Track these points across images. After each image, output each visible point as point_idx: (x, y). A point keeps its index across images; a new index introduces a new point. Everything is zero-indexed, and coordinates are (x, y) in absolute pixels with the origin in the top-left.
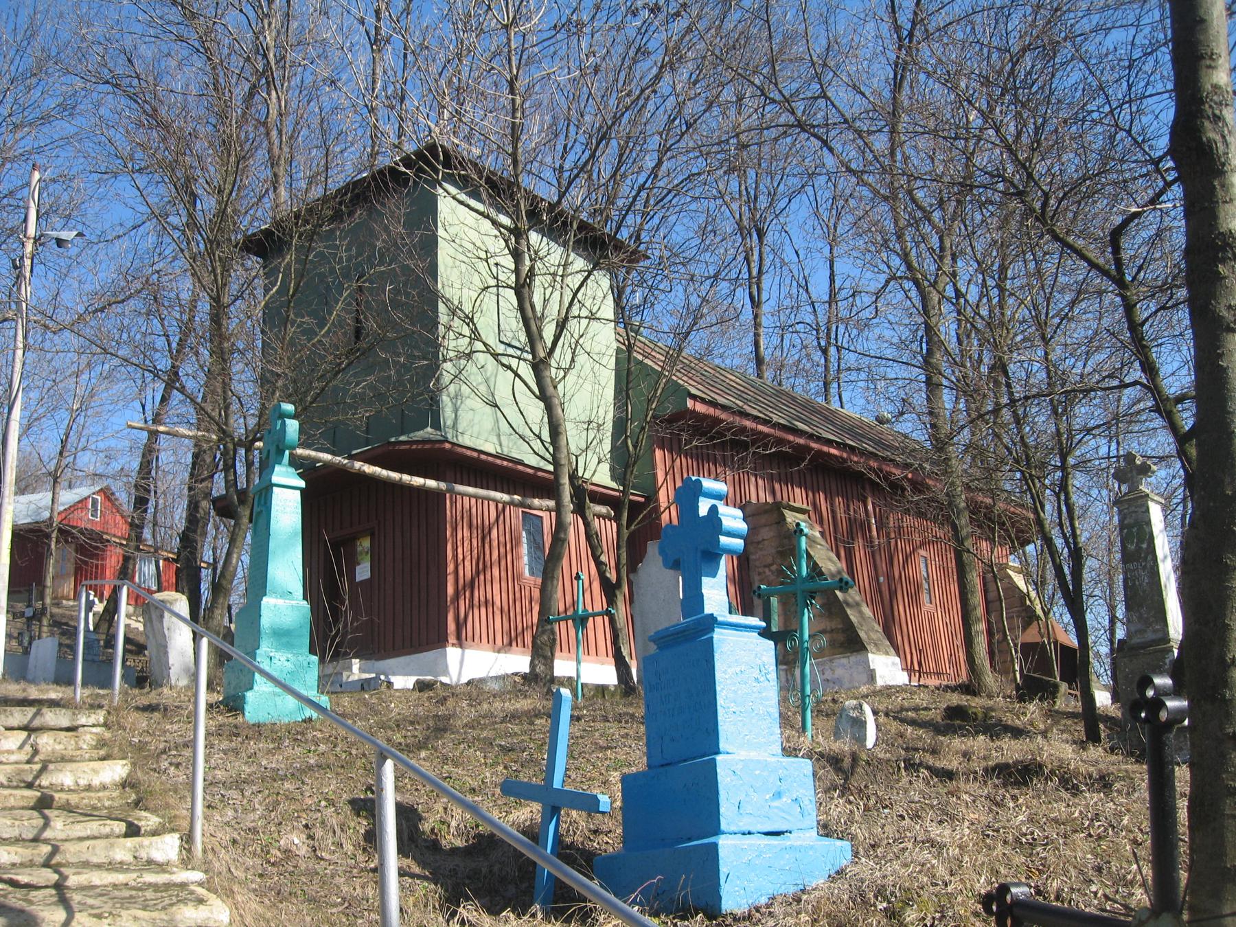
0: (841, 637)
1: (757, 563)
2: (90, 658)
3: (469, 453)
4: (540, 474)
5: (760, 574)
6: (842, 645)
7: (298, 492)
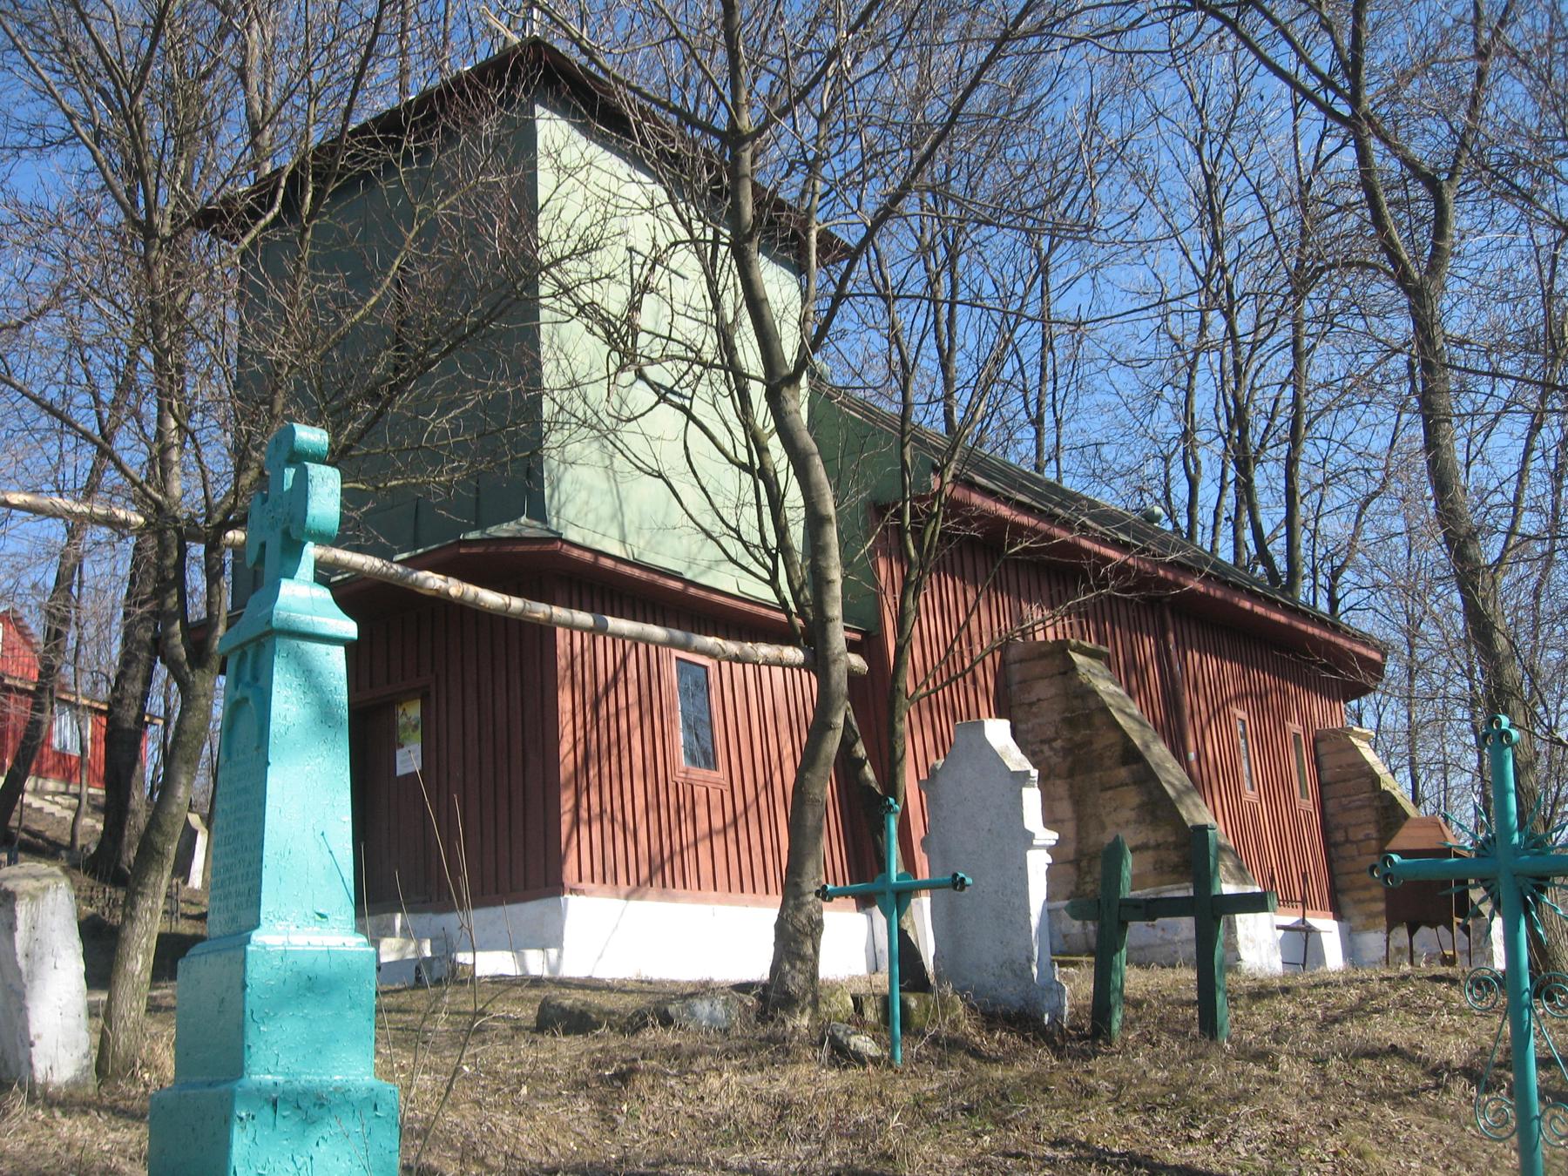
0: (1173, 857)
3: (576, 553)
4: (692, 591)
6: (1175, 869)
7: (339, 653)
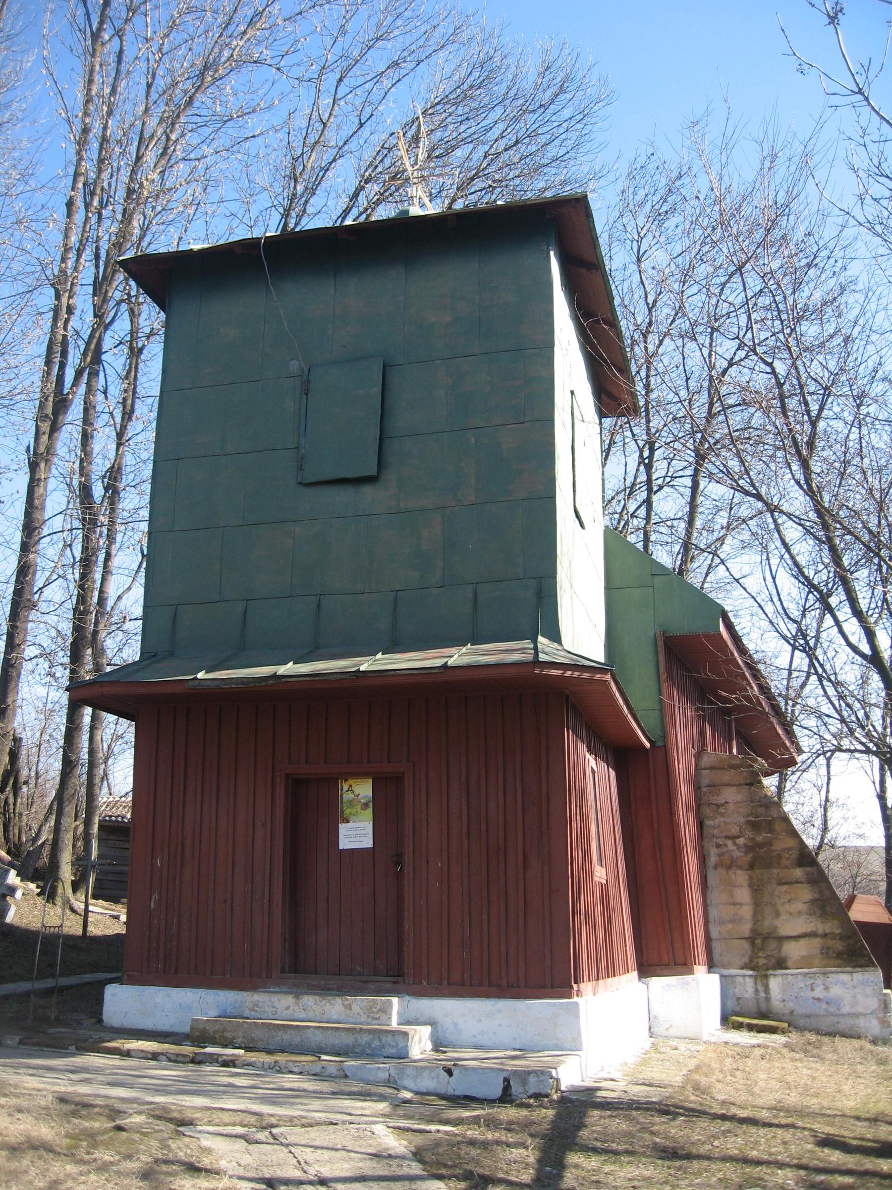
1: (715, 832)
2: (104, 837)
5: (718, 846)
6: (839, 955)
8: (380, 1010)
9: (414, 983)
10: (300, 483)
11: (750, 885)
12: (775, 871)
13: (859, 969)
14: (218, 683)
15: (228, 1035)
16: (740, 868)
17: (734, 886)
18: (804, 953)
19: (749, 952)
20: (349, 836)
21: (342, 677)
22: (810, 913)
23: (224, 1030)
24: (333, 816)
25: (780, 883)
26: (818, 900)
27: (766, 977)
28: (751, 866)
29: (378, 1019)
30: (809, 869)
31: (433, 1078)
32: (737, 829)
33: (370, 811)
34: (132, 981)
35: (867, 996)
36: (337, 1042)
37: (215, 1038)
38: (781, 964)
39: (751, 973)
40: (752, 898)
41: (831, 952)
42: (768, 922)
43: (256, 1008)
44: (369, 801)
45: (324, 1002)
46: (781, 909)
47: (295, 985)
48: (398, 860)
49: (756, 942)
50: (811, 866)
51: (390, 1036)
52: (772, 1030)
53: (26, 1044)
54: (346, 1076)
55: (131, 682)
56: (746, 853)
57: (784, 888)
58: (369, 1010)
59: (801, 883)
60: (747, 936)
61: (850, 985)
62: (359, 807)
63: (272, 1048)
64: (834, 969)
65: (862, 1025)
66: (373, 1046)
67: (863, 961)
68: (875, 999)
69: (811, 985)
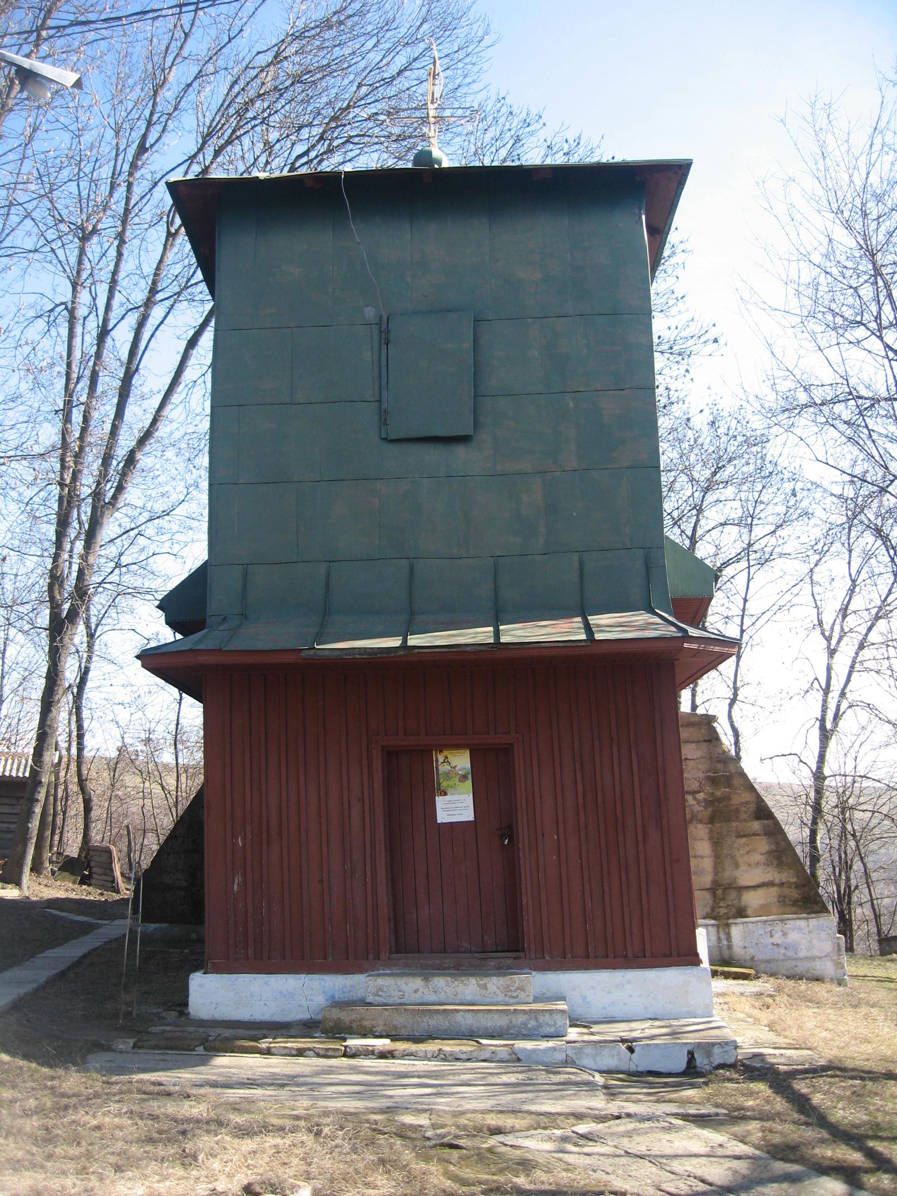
6: (795, 903)
8: (518, 988)
9: (536, 958)
10: (385, 439)
11: (711, 838)
12: (734, 824)
13: (814, 915)
14: (339, 653)
15: (367, 1024)
16: (701, 821)
17: (695, 840)
18: (762, 902)
19: (711, 902)
20: (447, 809)
21: (482, 648)
22: (768, 864)
23: (362, 1019)
24: (429, 788)
25: (739, 836)
26: (775, 851)
27: (728, 925)
28: (711, 820)
29: (517, 997)
30: (766, 821)
31: (613, 1056)
32: (697, 784)
33: (469, 783)
34: (218, 969)
35: (822, 941)
36: (489, 1024)
37: (351, 1028)
38: (741, 913)
39: (713, 922)
40: (713, 851)
41: (787, 901)
42: (728, 873)
43: (380, 993)
44: (468, 773)
45: (456, 983)
46: (740, 860)
47: (407, 966)
48: (509, 831)
49: (717, 892)
50: (768, 819)
51: (547, 1015)
52: (745, 977)
53: (139, 1048)
54: (519, 1060)
55: (230, 651)
56: (706, 807)
57: (743, 840)
58: (507, 989)
59: (758, 835)
60: (708, 887)
61: (807, 930)
62: (457, 779)
63: (417, 1034)
64: (790, 916)
65: (818, 967)
66: (530, 1026)
67: (817, 908)
68: (830, 943)
69: (771, 932)
